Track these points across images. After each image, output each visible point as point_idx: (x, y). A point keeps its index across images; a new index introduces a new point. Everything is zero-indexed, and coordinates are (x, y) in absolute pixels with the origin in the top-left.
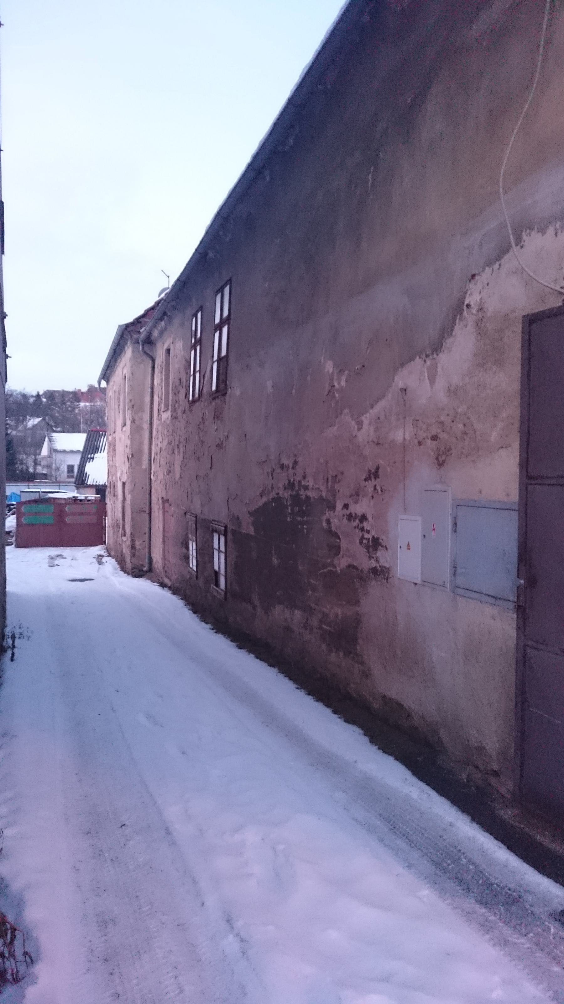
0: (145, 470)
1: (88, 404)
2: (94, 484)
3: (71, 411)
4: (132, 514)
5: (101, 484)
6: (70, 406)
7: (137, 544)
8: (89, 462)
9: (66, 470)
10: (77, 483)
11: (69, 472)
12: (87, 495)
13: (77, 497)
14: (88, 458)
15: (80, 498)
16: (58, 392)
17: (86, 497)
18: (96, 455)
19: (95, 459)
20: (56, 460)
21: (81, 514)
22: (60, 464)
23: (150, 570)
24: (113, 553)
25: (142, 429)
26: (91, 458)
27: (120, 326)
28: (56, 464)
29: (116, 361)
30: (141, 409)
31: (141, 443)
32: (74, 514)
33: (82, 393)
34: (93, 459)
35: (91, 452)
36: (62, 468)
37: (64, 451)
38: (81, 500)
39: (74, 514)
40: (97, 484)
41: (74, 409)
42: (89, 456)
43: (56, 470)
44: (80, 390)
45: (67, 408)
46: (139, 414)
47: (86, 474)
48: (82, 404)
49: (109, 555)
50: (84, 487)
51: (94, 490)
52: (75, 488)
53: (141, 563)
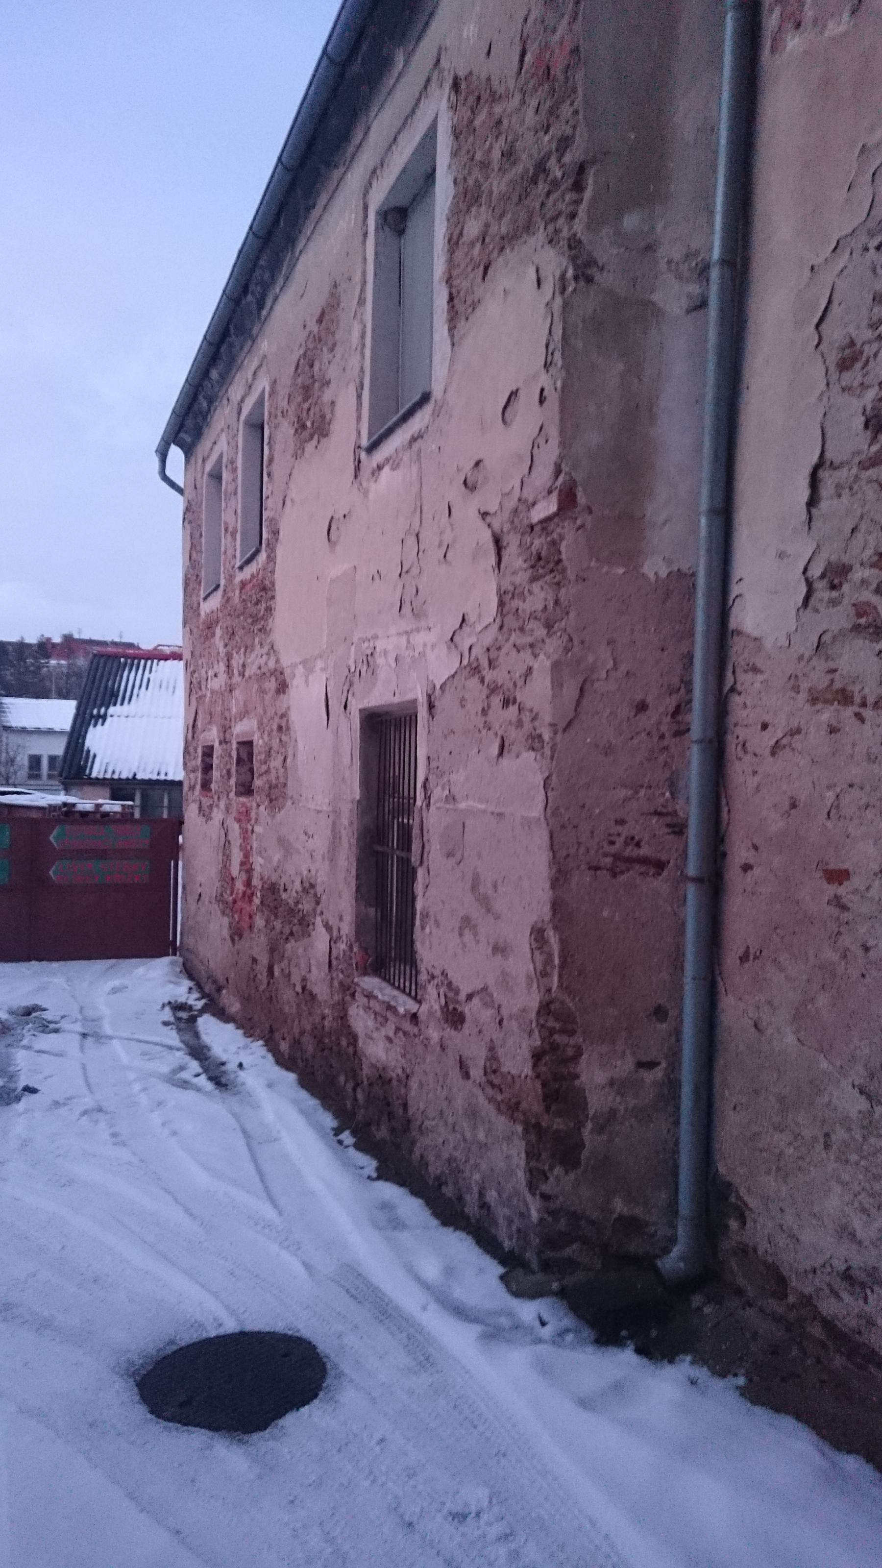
0: (682, 580)
1: (63, 662)
2: (108, 776)
3: (33, 672)
4: (555, 883)
5: (124, 776)
6: (33, 664)
7: (594, 1075)
8: (95, 726)
9: (26, 762)
10: (64, 775)
11: (31, 767)
12: (100, 801)
13: (74, 805)
14: (92, 716)
15: (80, 807)
16: (10, 644)
17: (98, 806)
18: (112, 710)
19: (109, 719)
20: (7, 745)
21: (102, 854)
22: (17, 753)
23: (707, 1276)
24: (232, 1003)
25: (648, 312)
26: (99, 716)
27: (157, 451)
28: (7, 752)
29: (274, 267)
30: (643, 178)
31: (635, 417)
32: (79, 854)
33: (54, 645)
34: (104, 718)
35: (99, 702)
36: (18, 759)
37: (24, 731)
38: (84, 814)
39: (79, 854)
40: (116, 776)
41: (39, 668)
42: (95, 712)
43: (7, 762)
44: (49, 639)
45: (27, 668)
46: (631, 221)
47: (88, 751)
48: (53, 662)
49: (222, 1015)
50: (84, 784)
51: (107, 792)
52: (61, 787)
53: (619, 1206)
